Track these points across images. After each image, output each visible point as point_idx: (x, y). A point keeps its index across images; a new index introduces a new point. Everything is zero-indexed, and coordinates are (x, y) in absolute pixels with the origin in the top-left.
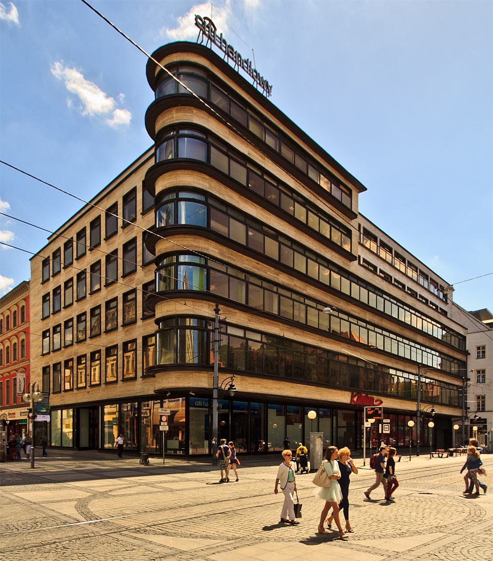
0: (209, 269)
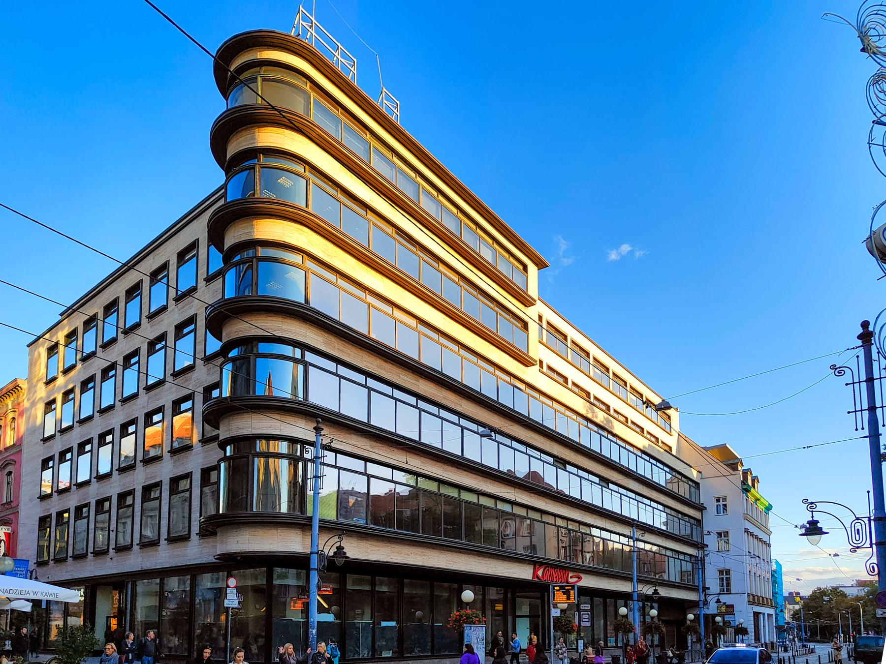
0: (306, 365)
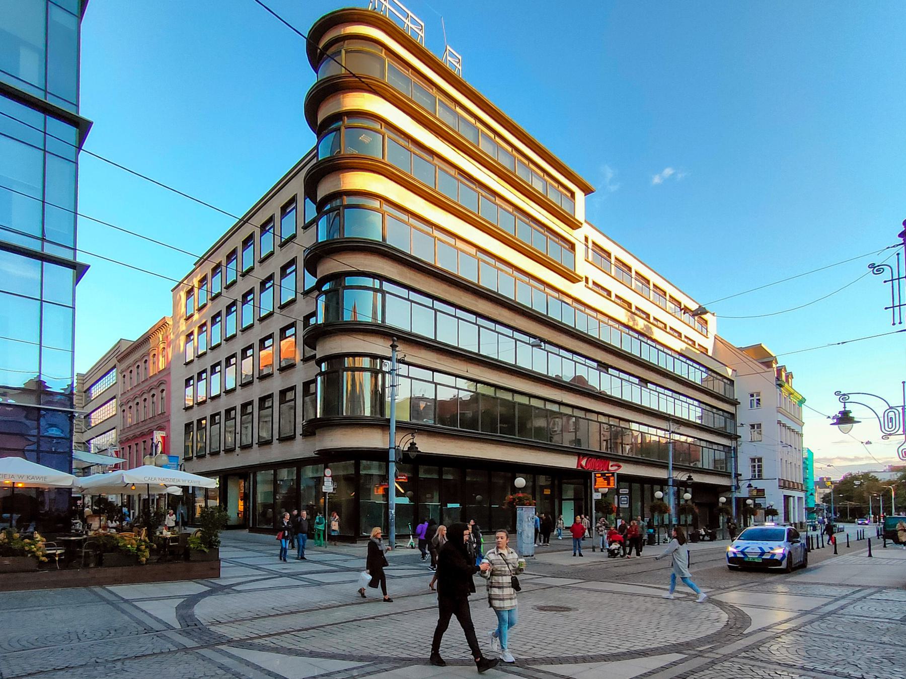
0: (384, 293)
